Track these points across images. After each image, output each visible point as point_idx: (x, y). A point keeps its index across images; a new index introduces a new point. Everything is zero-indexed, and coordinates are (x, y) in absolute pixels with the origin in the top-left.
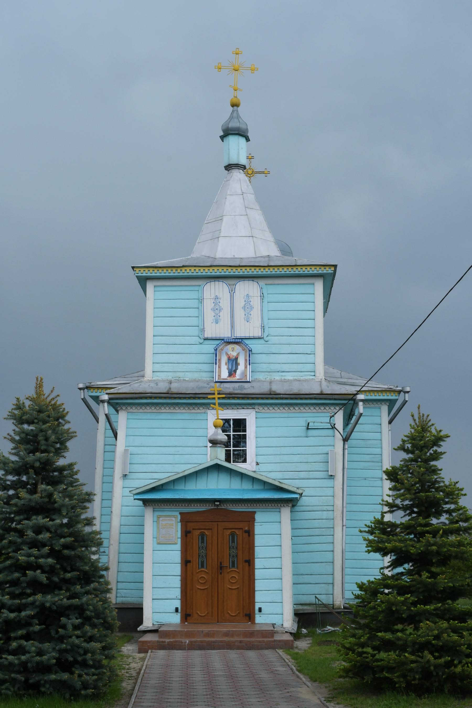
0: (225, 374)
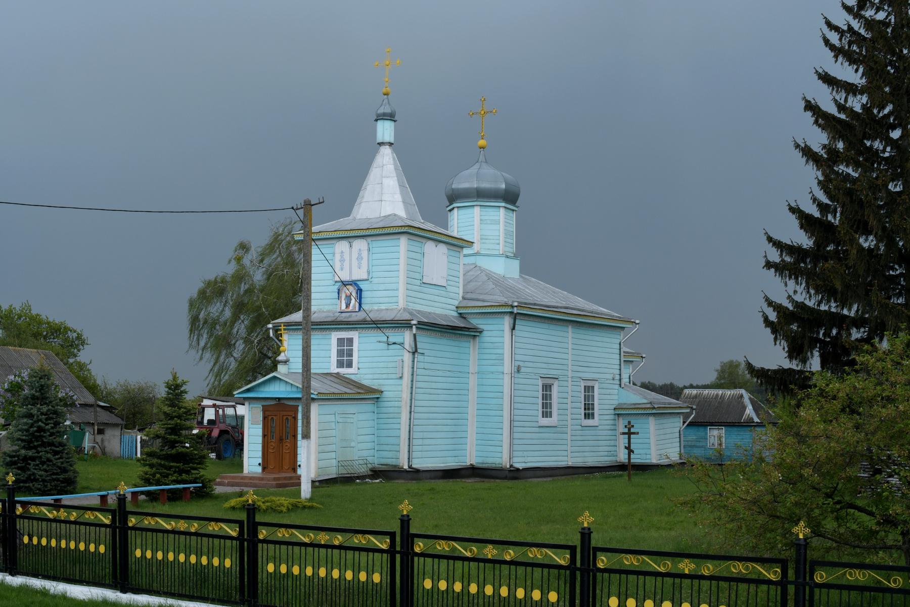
0: (344, 307)
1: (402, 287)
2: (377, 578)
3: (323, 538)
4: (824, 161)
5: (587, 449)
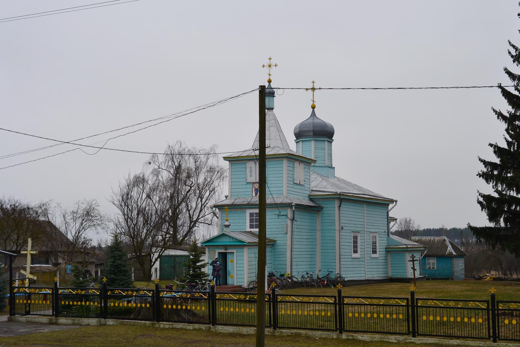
1: (285, 185)
2: (401, 317)
3: (375, 301)
4: (510, 120)
5: (374, 270)
